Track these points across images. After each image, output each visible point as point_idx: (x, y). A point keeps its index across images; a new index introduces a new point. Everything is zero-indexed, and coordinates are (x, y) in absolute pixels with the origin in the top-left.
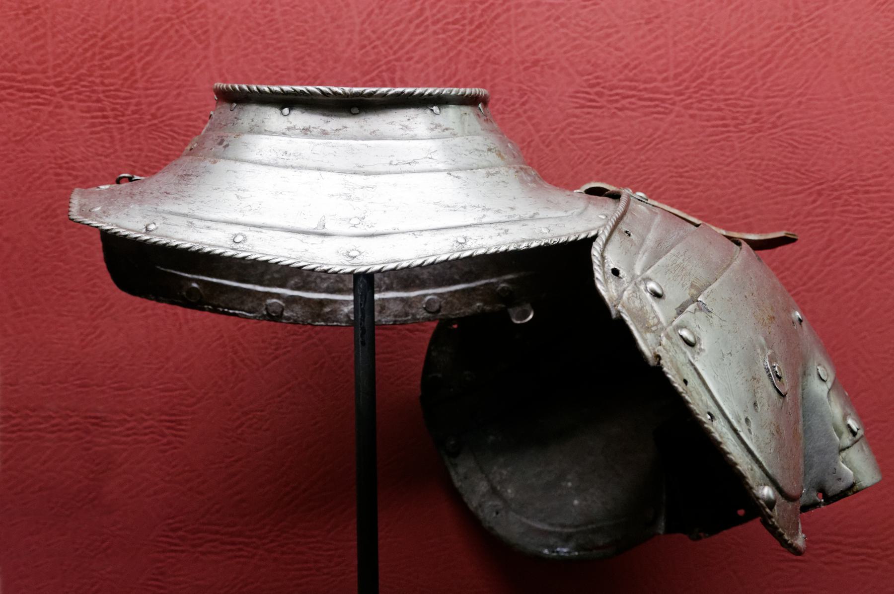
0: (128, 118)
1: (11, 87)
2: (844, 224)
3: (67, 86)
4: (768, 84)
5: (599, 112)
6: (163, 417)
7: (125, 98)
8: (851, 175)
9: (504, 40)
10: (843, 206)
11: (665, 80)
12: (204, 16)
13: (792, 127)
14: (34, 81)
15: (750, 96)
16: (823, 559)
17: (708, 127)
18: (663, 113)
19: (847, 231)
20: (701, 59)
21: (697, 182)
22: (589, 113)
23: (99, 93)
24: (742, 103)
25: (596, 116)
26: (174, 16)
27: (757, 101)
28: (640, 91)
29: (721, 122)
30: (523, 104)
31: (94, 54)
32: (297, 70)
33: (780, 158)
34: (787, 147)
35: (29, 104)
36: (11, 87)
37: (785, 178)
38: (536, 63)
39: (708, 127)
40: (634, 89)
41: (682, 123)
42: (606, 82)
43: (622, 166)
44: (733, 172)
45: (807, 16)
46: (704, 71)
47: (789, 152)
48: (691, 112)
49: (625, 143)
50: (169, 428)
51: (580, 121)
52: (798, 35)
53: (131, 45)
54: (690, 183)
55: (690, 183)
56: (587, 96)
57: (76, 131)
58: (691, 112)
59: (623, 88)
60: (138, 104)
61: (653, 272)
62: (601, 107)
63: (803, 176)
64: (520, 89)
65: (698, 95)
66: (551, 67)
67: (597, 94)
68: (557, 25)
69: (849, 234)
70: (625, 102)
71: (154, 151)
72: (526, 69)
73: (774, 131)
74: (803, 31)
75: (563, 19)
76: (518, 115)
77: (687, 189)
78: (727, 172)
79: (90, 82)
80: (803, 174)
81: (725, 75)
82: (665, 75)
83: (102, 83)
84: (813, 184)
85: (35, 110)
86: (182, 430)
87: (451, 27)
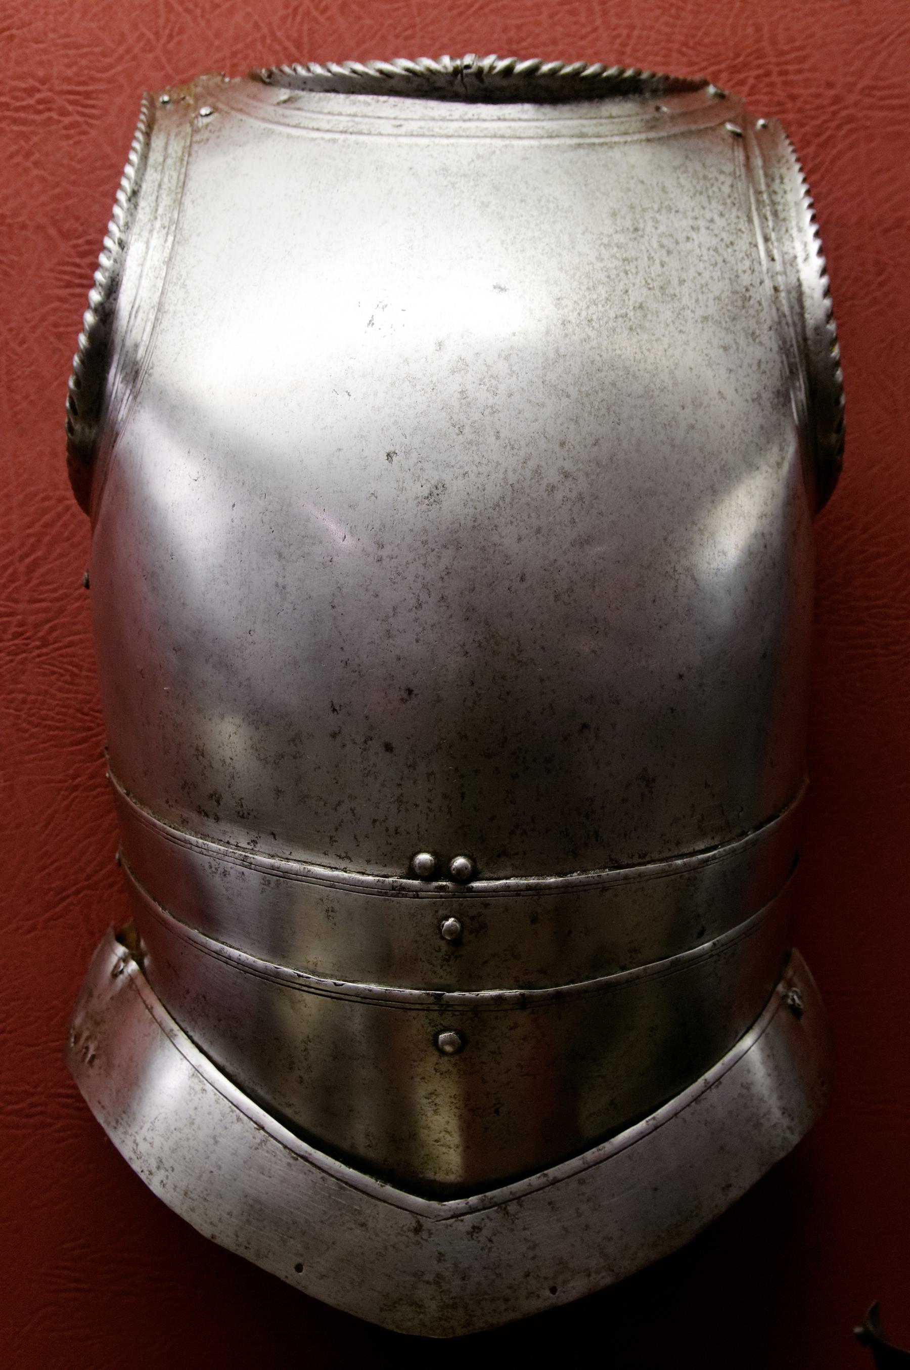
1: (17, 109)
13: (70, 645)
27: (21, 607)
33: (53, 691)
34: (62, 675)
36: (17, 109)
37: (60, 721)
47: (65, 682)
50: (71, 102)
51: (66, 306)
56: (78, 270)
61: (524, 148)
63: (86, 718)
66: (24, 227)
68: (29, 164)
73: (44, 650)
75: (37, 155)
80: (87, 715)
86: (93, 107)
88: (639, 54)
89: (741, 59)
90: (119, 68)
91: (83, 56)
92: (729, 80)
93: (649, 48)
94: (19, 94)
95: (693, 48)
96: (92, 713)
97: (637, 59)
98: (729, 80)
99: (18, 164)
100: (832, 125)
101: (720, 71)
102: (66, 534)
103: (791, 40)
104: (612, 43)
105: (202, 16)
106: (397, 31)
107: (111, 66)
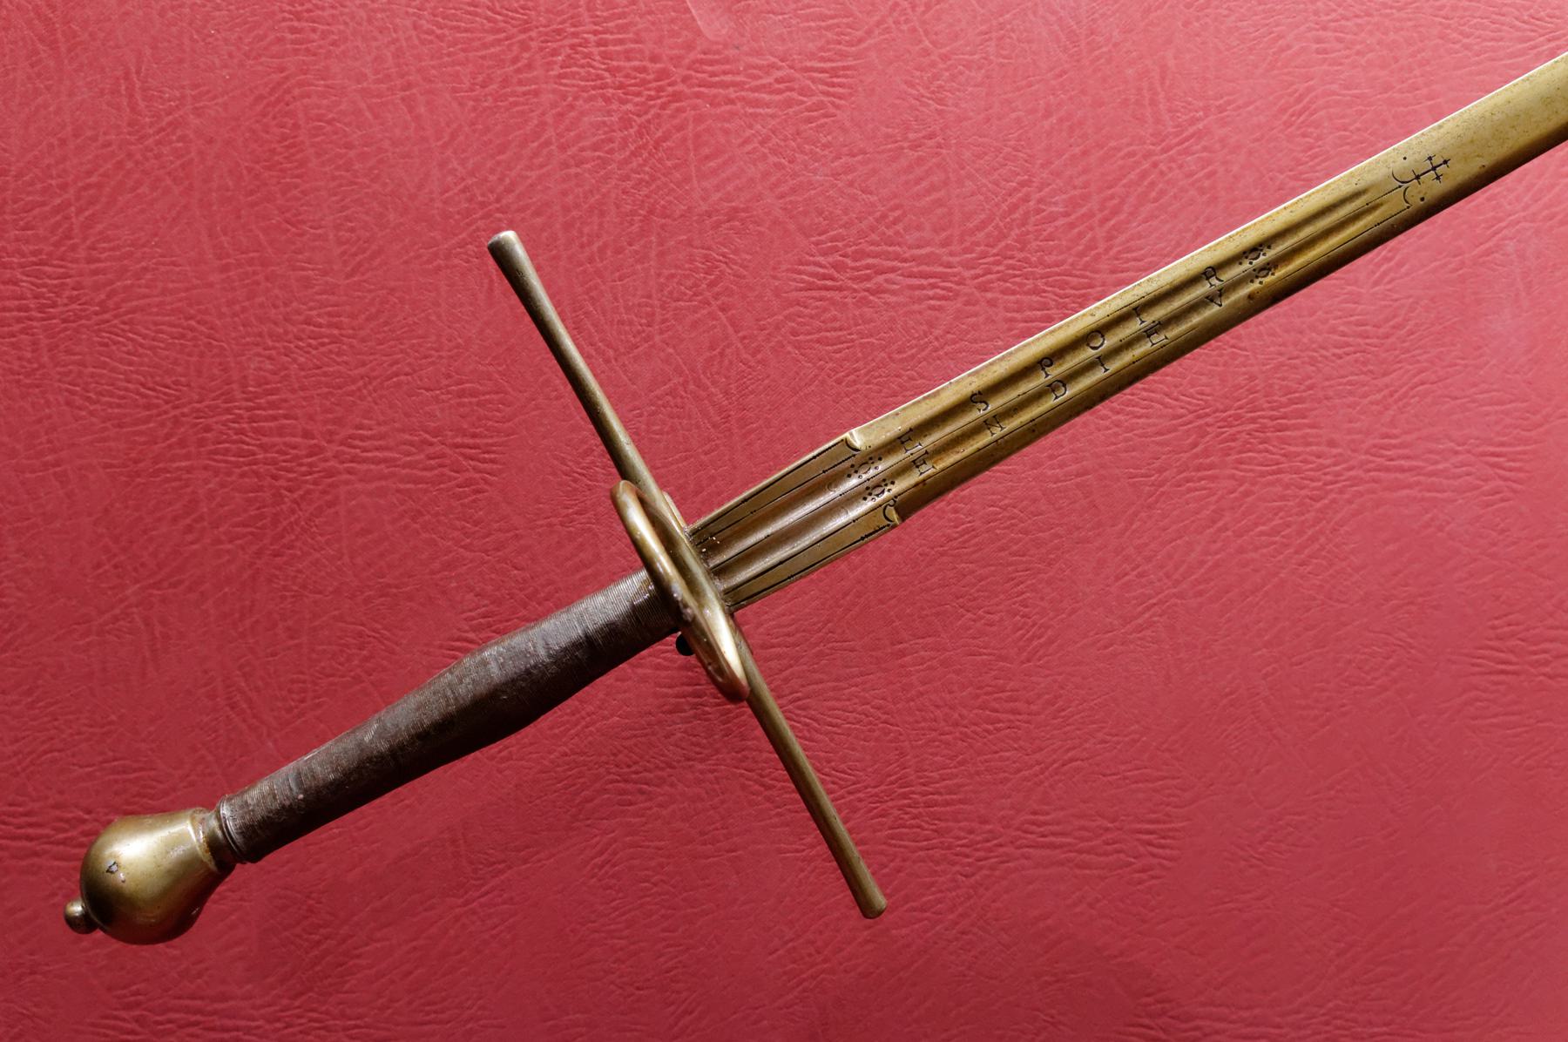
0: (60, 309)
2: (1241, 482)
4: (1115, 250)
5: (836, 295)
6: (459, 440)
7: (573, 75)
8: (1252, 402)
9: (677, 175)
10: (891, 828)
12: (182, 138)
14: (930, 259)
15: (1085, 268)
16: (1547, 670)
19: (1247, 494)
20: (1004, 207)
21: (1349, 37)
24: (1074, 281)
25: (833, 302)
26: (133, 138)
28: (905, 261)
30: (712, 285)
32: (338, 227)
38: (733, 214)
40: (198, 1011)
41: (976, 315)
43: (1226, 12)
44: (712, 771)
45: (1177, 135)
49: (883, 348)
52: (1162, 167)
53: (64, 187)
54: (1339, 40)
55: (1339, 40)
59: (877, 255)
62: (840, 289)
64: (707, 258)
67: (835, 266)
69: (1249, 500)
71: (104, 365)
72: (717, 226)
74: (1172, 160)
75: (775, 140)
76: (945, 58)
78: (702, 772)
84: (1190, 417)
86: (840, 85)
87: (588, 154)
90: (871, 41)
91: (828, 28)
94: (755, 72)
96: (1532, 20)
99: (406, 527)
102: (1154, 194)
105: (269, 735)
107: (860, 41)
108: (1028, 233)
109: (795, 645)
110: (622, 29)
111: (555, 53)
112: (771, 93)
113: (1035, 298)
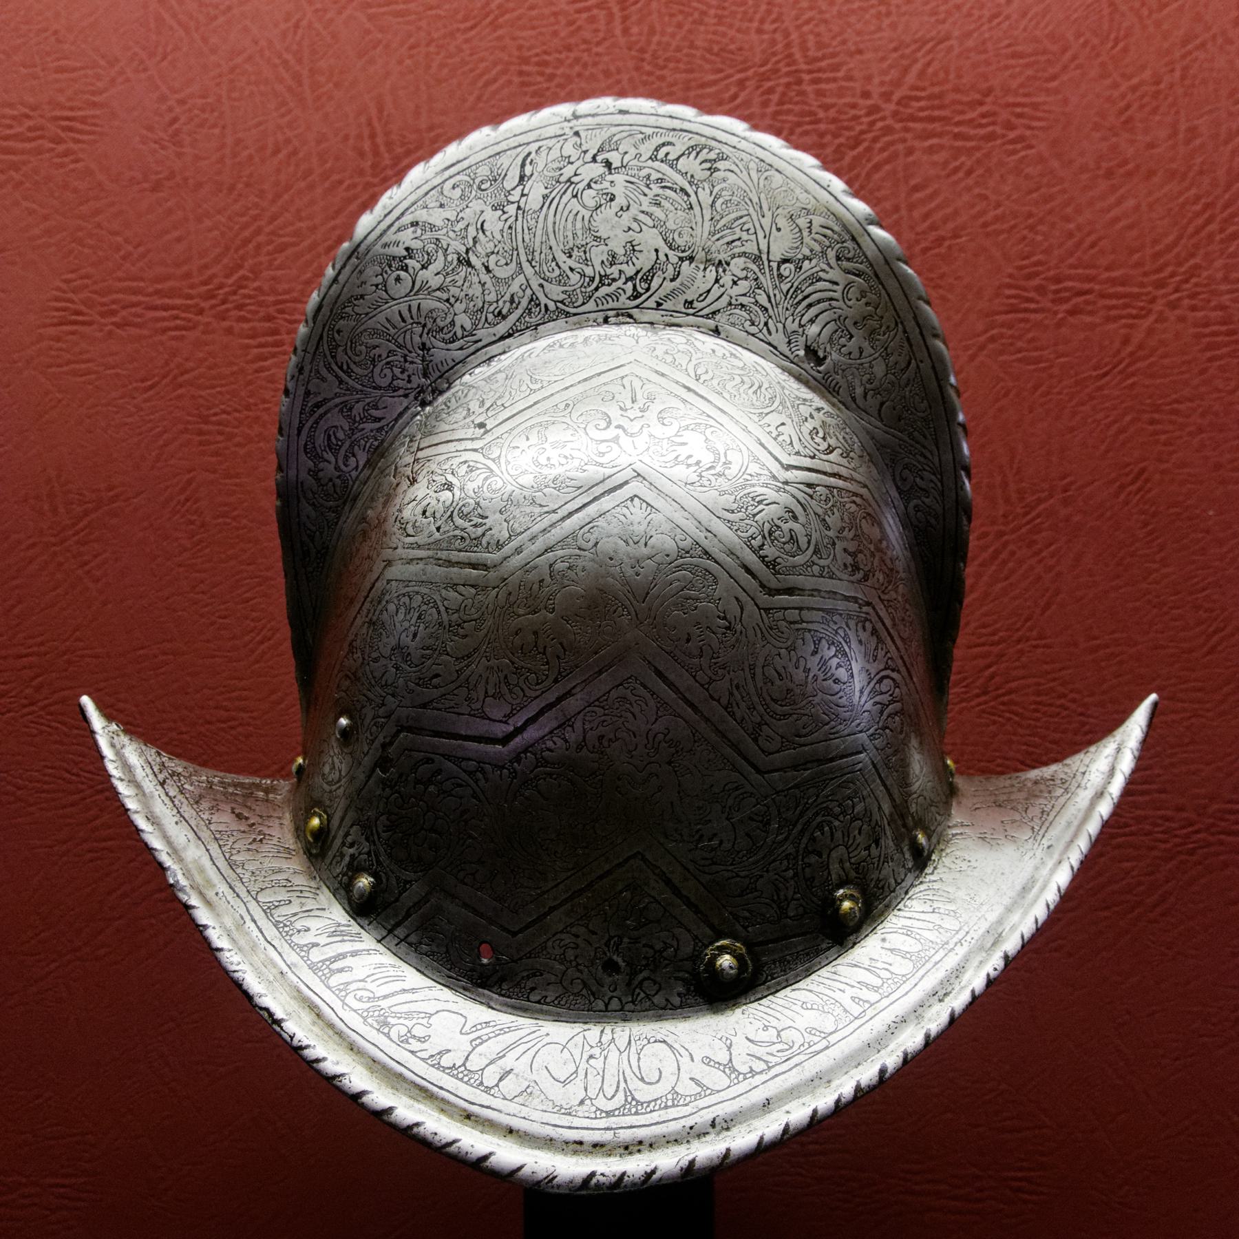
3: (220, 297)
7: (789, 112)
11: (910, 151)
14: (171, 293)
17: (1205, 336)
18: (185, 328)
21: (1181, 420)
22: (73, 333)
23: (268, 306)
29: (1224, 328)
31: (258, 247)
35: (164, 331)
36: (958, 124)
39: (1205, 336)
42: (1049, 269)
46: (243, 258)
48: (226, 324)
50: (65, 129)
57: (235, 368)
58: (226, 324)
59: (23, 152)
60: (765, 104)
65: (1187, 286)
67: (84, 302)
70: (971, 115)
76: (182, 102)
77: (1167, 432)
79: (255, 289)
81: (276, 263)
82: (185, 268)
83: (273, 291)
85: (174, 338)
88: (661, 62)
89: (769, 66)
91: (1027, 66)
92: (758, 88)
93: (669, 54)
95: (717, 55)
97: (656, 66)
98: (758, 88)
100: (870, 136)
101: (747, 79)
103: (592, 20)
104: (781, 14)
106: (1007, 23)
108: (261, 263)
109: (998, 643)
110: (835, 68)
111: (771, 91)
112: (23, 141)
113: (267, 325)
